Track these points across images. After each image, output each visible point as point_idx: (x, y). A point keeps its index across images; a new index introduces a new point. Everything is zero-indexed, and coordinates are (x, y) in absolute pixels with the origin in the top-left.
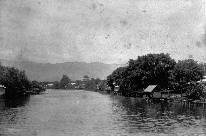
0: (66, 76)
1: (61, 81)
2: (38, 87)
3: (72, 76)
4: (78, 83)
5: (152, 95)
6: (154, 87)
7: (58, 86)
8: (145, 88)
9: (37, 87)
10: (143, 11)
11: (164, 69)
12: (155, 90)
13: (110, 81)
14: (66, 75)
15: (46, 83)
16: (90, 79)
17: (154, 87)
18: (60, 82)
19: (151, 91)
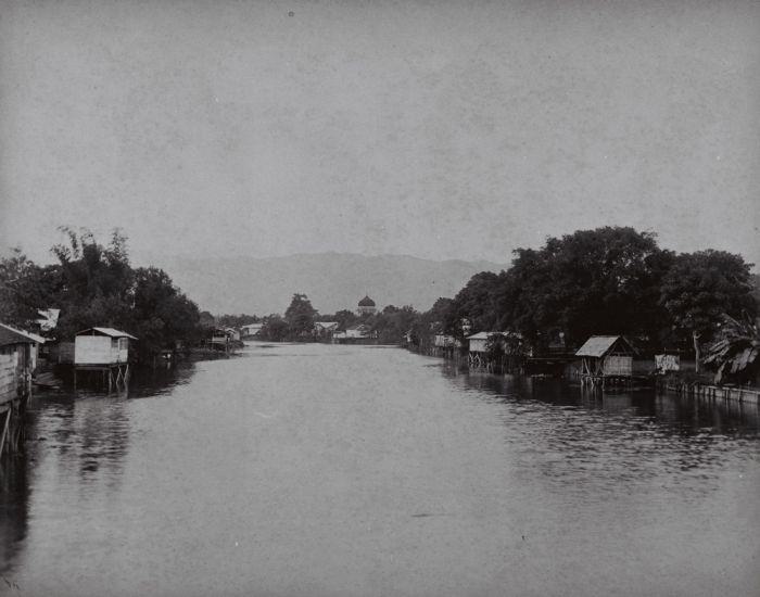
0: (303, 299)
1: (287, 314)
2: (222, 336)
3: (562, 335)
4: (345, 319)
5: (327, 319)
6: (608, 342)
7: (276, 331)
8: (578, 348)
9: (218, 336)
10: (57, 251)
11: (624, 272)
12: (615, 350)
13: (452, 315)
14: (304, 296)
15: (241, 322)
16: (380, 308)
17: (608, 342)
18: (283, 316)
19: (599, 356)
